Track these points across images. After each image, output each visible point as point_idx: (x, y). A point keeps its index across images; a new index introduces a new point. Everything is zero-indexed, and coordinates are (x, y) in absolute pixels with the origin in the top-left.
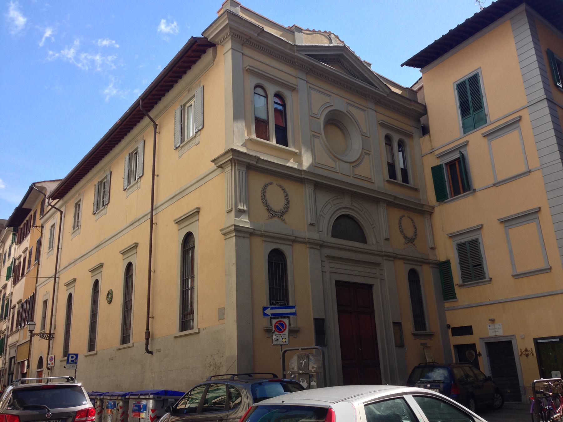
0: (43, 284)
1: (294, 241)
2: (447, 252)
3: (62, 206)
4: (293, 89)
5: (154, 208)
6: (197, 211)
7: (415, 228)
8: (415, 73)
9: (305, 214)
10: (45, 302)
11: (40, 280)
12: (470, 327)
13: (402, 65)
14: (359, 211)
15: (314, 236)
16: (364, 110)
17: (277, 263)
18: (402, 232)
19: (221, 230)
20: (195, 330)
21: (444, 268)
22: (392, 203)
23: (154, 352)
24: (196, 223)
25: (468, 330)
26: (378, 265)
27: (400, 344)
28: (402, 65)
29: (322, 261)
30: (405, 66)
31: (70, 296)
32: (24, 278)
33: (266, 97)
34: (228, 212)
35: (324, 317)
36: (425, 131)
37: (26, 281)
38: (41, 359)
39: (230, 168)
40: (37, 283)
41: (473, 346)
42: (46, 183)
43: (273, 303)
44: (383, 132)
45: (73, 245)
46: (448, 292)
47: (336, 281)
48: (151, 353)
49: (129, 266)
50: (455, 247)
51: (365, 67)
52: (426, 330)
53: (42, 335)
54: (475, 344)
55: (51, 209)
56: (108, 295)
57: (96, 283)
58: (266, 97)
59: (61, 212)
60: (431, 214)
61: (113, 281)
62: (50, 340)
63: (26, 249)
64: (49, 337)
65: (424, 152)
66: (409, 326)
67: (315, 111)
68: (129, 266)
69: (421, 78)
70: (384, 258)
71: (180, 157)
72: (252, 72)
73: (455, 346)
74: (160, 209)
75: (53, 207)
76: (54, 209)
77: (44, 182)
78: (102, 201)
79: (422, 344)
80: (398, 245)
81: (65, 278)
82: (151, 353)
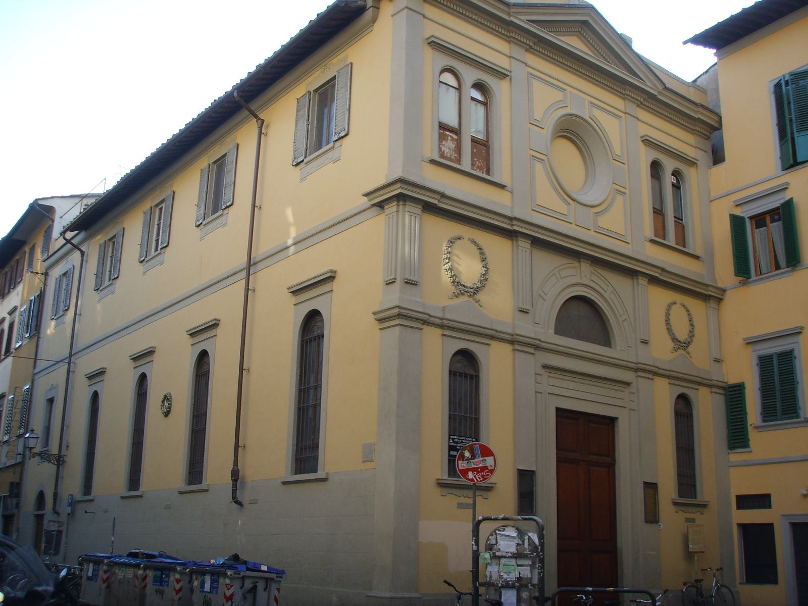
0: (46, 371)
1: (492, 336)
2: (743, 371)
3: (82, 242)
4: (501, 75)
5: (252, 263)
6: (331, 278)
7: (692, 325)
8: (707, 57)
9: (501, 288)
10: (51, 401)
11: (41, 365)
12: (768, 496)
13: (685, 43)
14: (611, 292)
15: (526, 328)
16: (619, 117)
17: (465, 371)
18: (669, 330)
19: (374, 313)
20: (320, 474)
21: (734, 395)
22: (660, 279)
23: (245, 502)
24: (330, 294)
25: (762, 501)
26: (628, 384)
27: (652, 516)
28: (685, 43)
29: (536, 374)
30: (689, 44)
31: (95, 396)
32: (10, 360)
33: (459, 89)
34: (389, 283)
35: (534, 469)
36: (717, 157)
37: (14, 363)
38: (41, 496)
39: (395, 208)
40: (34, 367)
41: (769, 527)
42: (55, 199)
43: (452, 439)
44: (645, 156)
45: (98, 311)
46: (737, 436)
47: (558, 409)
48: (239, 503)
49: (203, 357)
50: (755, 361)
51: (626, 42)
52: (695, 498)
53: (44, 456)
54: (772, 525)
55: (65, 245)
56: (163, 402)
57: (143, 378)
58: (459, 89)
59: (83, 253)
60: (719, 300)
61: (173, 377)
62: (58, 466)
63: (15, 309)
64: (58, 461)
65: (714, 195)
66: (668, 488)
67: (538, 115)
68: (203, 357)
69: (716, 64)
70: (640, 374)
71: (303, 179)
72: (436, 45)
73: (739, 525)
74: (260, 266)
75: (68, 241)
76: (69, 246)
77: (52, 198)
78: (157, 244)
79: (688, 520)
80: (661, 351)
81: (86, 364)
82: (239, 503)
